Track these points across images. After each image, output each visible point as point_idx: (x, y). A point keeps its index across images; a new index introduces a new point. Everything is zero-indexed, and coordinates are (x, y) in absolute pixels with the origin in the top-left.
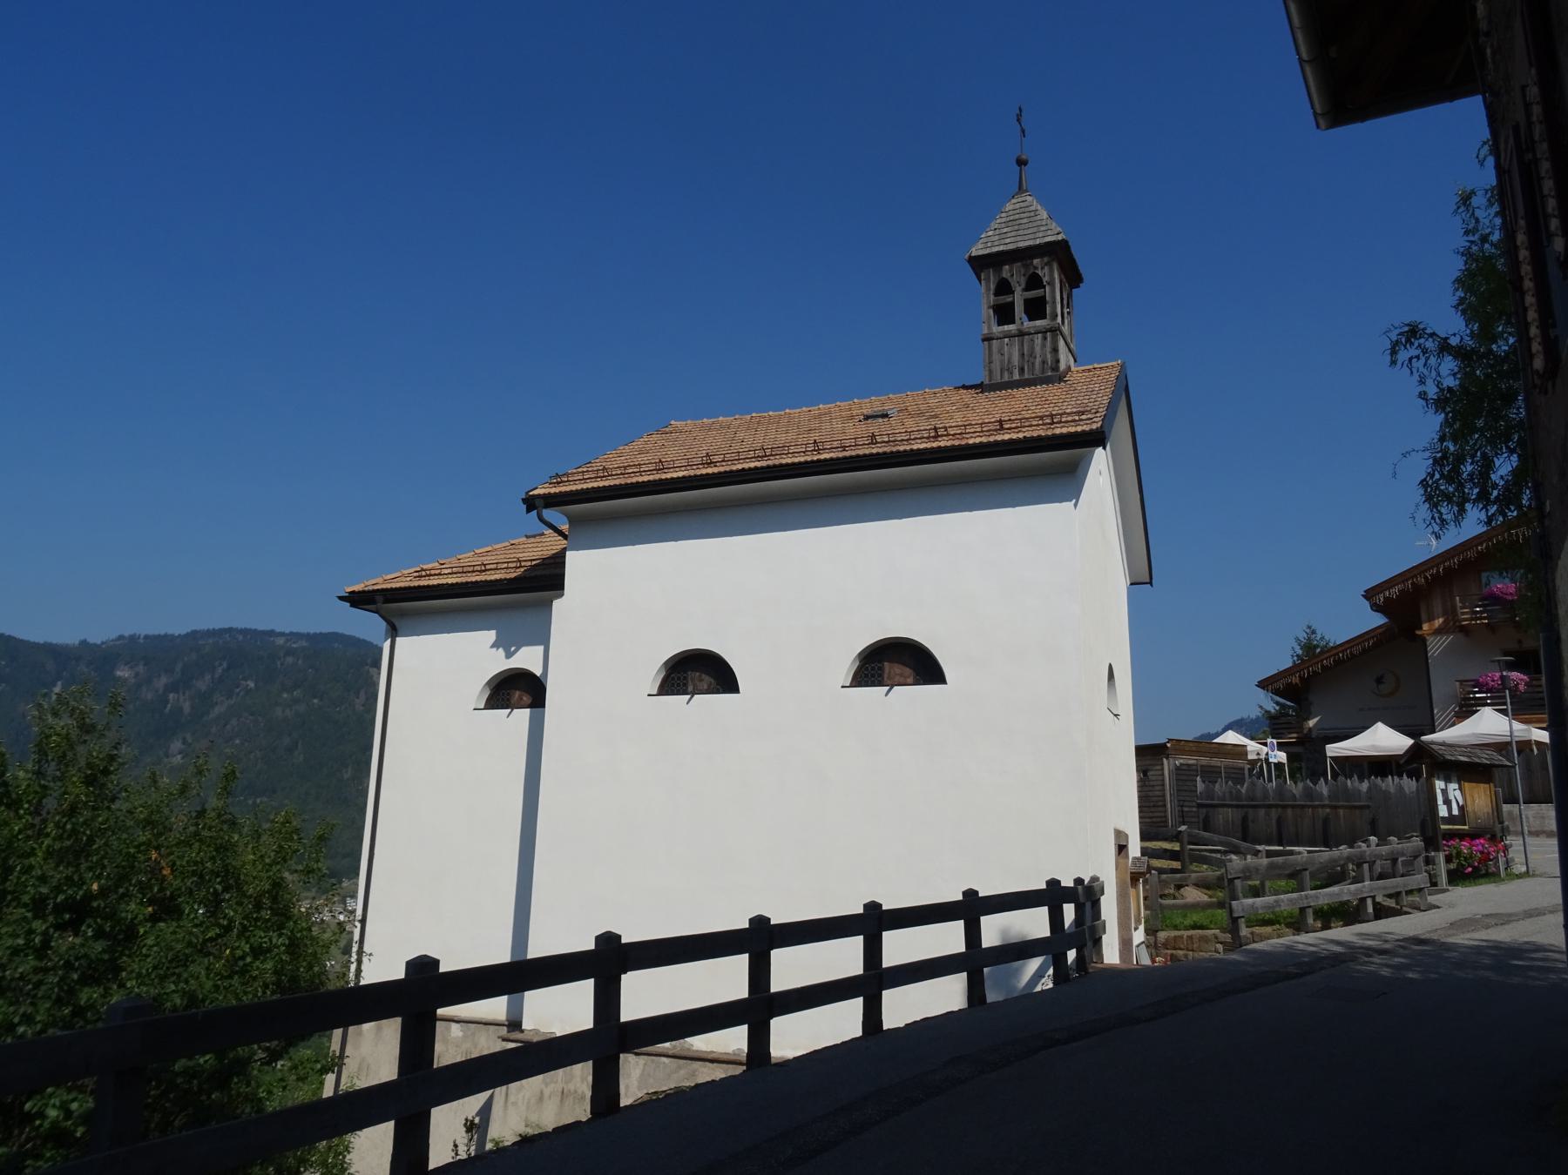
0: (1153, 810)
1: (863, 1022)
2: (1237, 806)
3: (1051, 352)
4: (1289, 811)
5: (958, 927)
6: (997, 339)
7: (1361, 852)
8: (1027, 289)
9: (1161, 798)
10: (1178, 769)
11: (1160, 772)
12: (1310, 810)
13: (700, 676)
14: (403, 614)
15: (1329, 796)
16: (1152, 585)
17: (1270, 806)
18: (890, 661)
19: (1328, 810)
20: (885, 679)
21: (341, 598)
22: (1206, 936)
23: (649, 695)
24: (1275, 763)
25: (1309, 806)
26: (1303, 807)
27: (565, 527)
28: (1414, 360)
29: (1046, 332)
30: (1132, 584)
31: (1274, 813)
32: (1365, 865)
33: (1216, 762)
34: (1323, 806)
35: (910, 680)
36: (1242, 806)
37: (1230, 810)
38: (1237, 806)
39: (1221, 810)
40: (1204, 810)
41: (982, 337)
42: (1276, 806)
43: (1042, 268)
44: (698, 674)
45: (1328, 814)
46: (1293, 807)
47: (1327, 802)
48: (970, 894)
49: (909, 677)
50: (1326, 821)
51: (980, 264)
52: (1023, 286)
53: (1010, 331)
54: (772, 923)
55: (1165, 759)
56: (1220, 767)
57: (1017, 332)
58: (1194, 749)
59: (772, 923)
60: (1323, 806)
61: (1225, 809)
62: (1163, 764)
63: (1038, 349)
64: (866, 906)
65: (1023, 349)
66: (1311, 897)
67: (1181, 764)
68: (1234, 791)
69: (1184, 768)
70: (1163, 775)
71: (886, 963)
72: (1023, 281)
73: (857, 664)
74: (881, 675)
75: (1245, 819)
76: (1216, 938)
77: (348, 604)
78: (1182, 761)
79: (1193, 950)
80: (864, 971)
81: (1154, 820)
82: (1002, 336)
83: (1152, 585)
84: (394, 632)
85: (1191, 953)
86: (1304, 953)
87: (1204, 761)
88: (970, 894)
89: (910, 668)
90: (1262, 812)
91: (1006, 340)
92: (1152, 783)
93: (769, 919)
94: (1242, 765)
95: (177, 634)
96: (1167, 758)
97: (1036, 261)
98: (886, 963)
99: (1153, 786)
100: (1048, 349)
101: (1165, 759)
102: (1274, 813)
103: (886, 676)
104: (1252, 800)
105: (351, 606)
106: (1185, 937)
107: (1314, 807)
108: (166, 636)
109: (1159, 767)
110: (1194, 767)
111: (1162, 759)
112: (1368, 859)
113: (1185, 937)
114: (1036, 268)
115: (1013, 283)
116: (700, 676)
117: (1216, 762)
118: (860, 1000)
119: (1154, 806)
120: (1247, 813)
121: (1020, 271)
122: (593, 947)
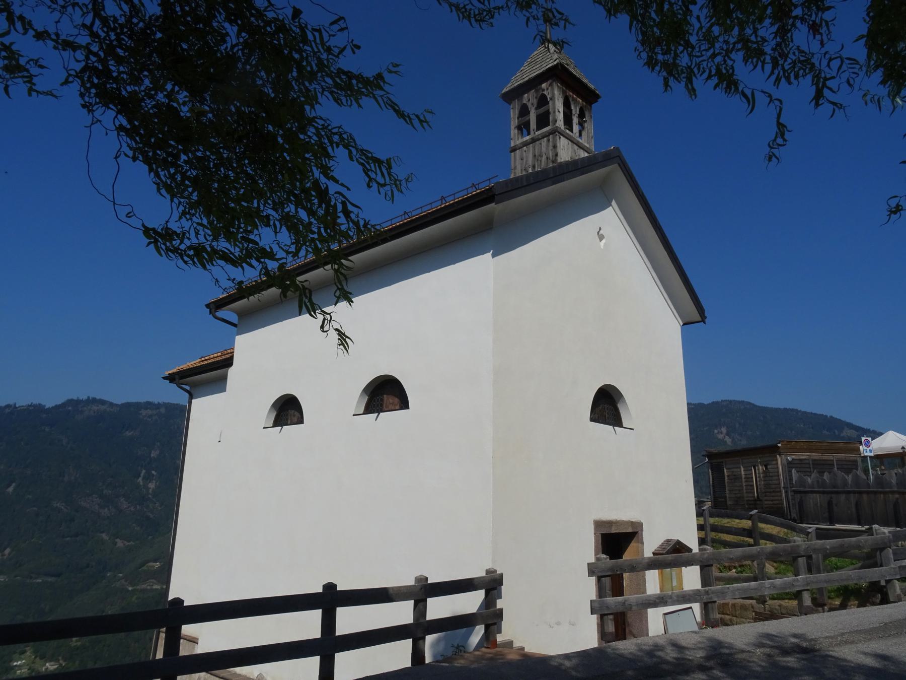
0: (773, 494)
1: (319, 676)
2: (824, 493)
3: (552, 150)
4: (865, 496)
5: (316, 616)
6: (519, 149)
7: (792, 547)
8: (536, 109)
9: (778, 486)
10: (789, 463)
11: (776, 466)
12: (882, 495)
13: (294, 413)
14: (194, 385)
15: (897, 484)
16: (705, 323)
17: (849, 492)
18: (387, 394)
19: (897, 496)
20: (384, 407)
21: (165, 378)
22: (745, 605)
23: (264, 428)
24: (871, 457)
25: (881, 493)
26: (875, 493)
27: (235, 321)
28: (515, 13)
29: (549, 136)
30: (684, 325)
31: (853, 498)
32: (800, 560)
33: (828, 456)
34: (893, 492)
35: (397, 407)
36: (828, 493)
37: (818, 495)
38: (824, 493)
39: (811, 495)
40: (799, 496)
41: (510, 150)
42: (854, 492)
43: (547, 89)
44: (293, 411)
45: (897, 499)
46: (868, 493)
47: (896, 489)
48: (330, 587)
49: (397, 405)
50: (896, 504)
51: (510, 97)
52: (535, 106)
53: (527, 140)
54: (338, 589)
55: (778, 456)
56: (833, 460)
57: (531, 140)
58: (805, 447)
59: (338, 589)
60: (893, 492)
61: (814, 495)
62: (777, 460)
63: (544, 149)
64: (324, 586)
65: (535, 151)
66: (713, 593)
67: (793, 459)
68: (820, 480)
69: (796, 462)
70: (778, 468)
71: (339, 632)
72: (535, 102)
73: (366, 398)
74: (382, 405)
75: (830, 503)
76: (753, 607)
77: (168, 381)
78: (793, 457)
79: (736, 617)
80: (163, 657)
81: (775, 502)
82: (522, 146)
83: (705, 323)
84: (191, 397)
85: (735, 618)
86: (621, 656)
87: (816, 456)
88: (330, 587)
89: (397, 397)
90: (843, 497)
91: (525, 148)
92: (771, 474)
93: (183, 601)
94: (855, 458)
95: (51, 407)
96: (780, 455)
97: (544, 85)
98: (339, 632)
99: (772, 477)
100: (551, 147)
101: (778, 456)
102: (853, 498)
103: (384, 405)
104: (834, 488)
105: (170, 382)
106: (730, 605)
107: (885, 493)
108: (713, 403)
109: (774, 462)
110: (807, 461)
111: (776, 456)
112: (803, 553)
113: (730, 605)
114: (543, 90)
115: (529, 105)
116: (294, 413)
117: (828, 456)
118: (317, 658)
119: (774, 492)
120: (831, 498)
121: (534, 96)
122: (321, 591)
